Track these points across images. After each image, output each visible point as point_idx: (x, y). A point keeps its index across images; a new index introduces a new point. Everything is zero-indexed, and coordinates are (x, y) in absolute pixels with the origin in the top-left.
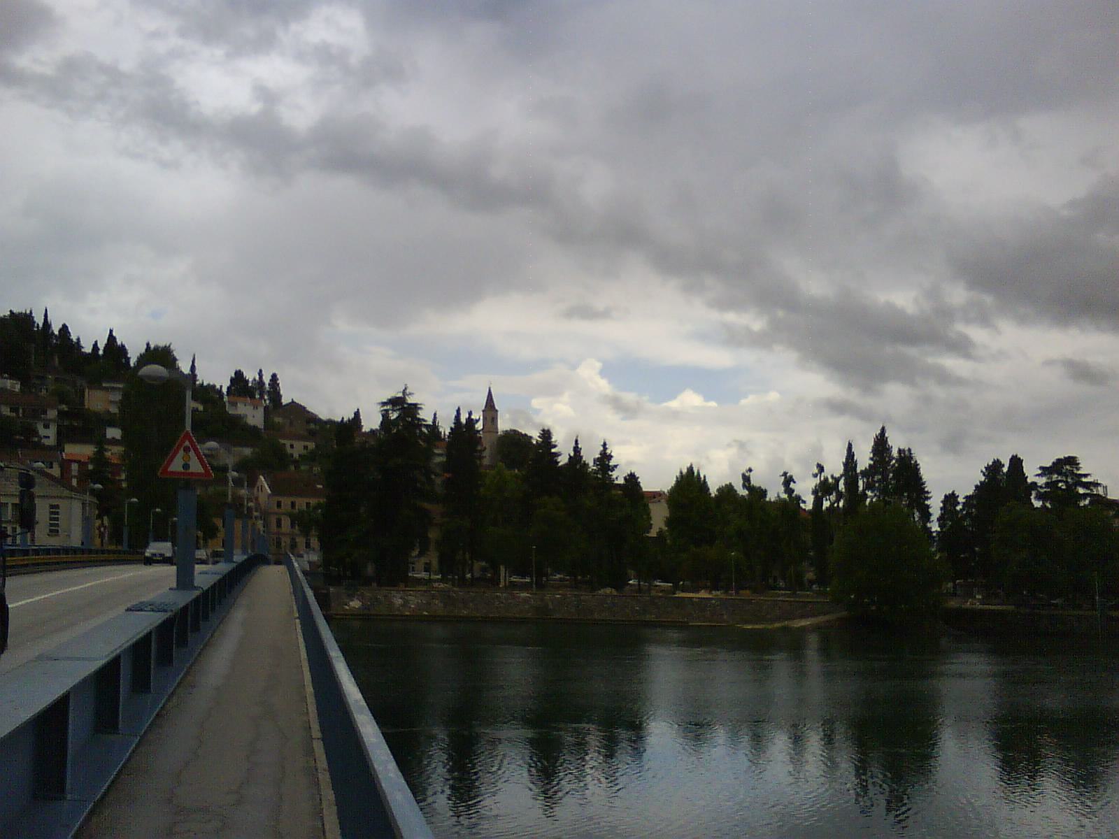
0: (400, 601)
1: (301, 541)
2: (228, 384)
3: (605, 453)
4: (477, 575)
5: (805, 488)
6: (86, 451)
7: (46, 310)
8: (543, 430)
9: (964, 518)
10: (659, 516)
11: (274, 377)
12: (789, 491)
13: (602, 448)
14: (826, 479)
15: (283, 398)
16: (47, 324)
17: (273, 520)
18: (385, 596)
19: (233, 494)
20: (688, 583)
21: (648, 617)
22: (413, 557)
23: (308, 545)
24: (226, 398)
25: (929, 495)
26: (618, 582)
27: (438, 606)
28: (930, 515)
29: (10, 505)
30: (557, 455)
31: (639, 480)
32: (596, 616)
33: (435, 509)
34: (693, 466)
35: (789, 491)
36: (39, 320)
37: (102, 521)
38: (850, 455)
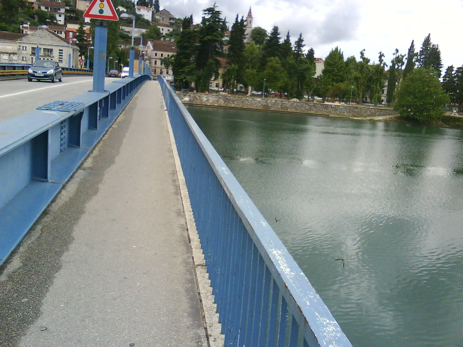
0: (206, 99)
1: (165, 71)
3: (301, 39)
4: (238, 89)
5: (388, 60)
6: (76, 27)
8: (275, 27)
9: (455, 77)
10: (319, 69)
12: (381, 61)
13: (299, 37)
14: (399, 56)
15: (160, 8)
18: (199, 97)
20: (329, 98)
21: (312, 112)
22: (212, 81)
23: (167, 73)
24: (136, 7)
25: (442, 66)
26: (299, 96)
27: (222, 102)
28: (441, 75)
30: (279, 38)
32: (289, 110)
33: (223, 60)
34: (338, 47)
35: (381, 61)
37: (82, 58)
38: (412, 46)
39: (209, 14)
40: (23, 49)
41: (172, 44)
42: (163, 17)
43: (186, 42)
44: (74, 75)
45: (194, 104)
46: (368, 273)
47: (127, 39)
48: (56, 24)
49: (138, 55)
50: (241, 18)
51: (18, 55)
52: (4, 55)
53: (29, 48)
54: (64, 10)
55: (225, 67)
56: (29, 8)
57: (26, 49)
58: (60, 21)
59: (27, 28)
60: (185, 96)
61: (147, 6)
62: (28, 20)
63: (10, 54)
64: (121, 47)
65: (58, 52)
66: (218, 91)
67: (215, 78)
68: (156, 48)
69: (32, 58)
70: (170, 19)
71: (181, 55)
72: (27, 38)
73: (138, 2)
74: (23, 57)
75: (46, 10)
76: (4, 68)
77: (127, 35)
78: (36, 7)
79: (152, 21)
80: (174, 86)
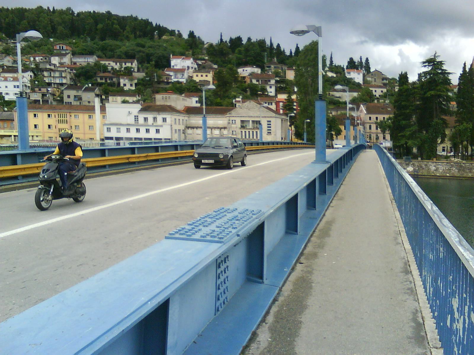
1: (381, 136)
2: (347, 64)
7: (271, 38)
11: (367, 59)
16: (271, 44)
17: (367, 126)
18: (426, 165)
19: (349, 114)
23: (384, 138)
24: (346, 71)
27: (455, 171)
33: (451, 120)
36: (268, 43)
39: (429, 66)
40: (232, 122)
41: (387, 105)
42: (375, 78)
43: (404, 101)
44: (263, 151)
45: (420, 175)
47: (338, 104)
48: (267, 95)
49: (353, 122)
50: (469, 67)
51: (228, 129)
55: (455, 127)
56: (241, 82)
57: (235, 123)
58: (271, 92)
59: (239, 101)
60: (408, 165)
61: (357, 69)
62: (240, 93)
63: (221, 128)
64: (331, 113)
65: (266, 123)
66: (447, 157)
67: (441, 141)
68: (369, 111)
70: (383, 79)
71: (400, 116)
73: (347, 66)
74: (233, 131)
75: (258, 83)
76: (13, 159)
77: (339, 101)
78: (248, 81)
79: (363, 83)
80: (394, 154)
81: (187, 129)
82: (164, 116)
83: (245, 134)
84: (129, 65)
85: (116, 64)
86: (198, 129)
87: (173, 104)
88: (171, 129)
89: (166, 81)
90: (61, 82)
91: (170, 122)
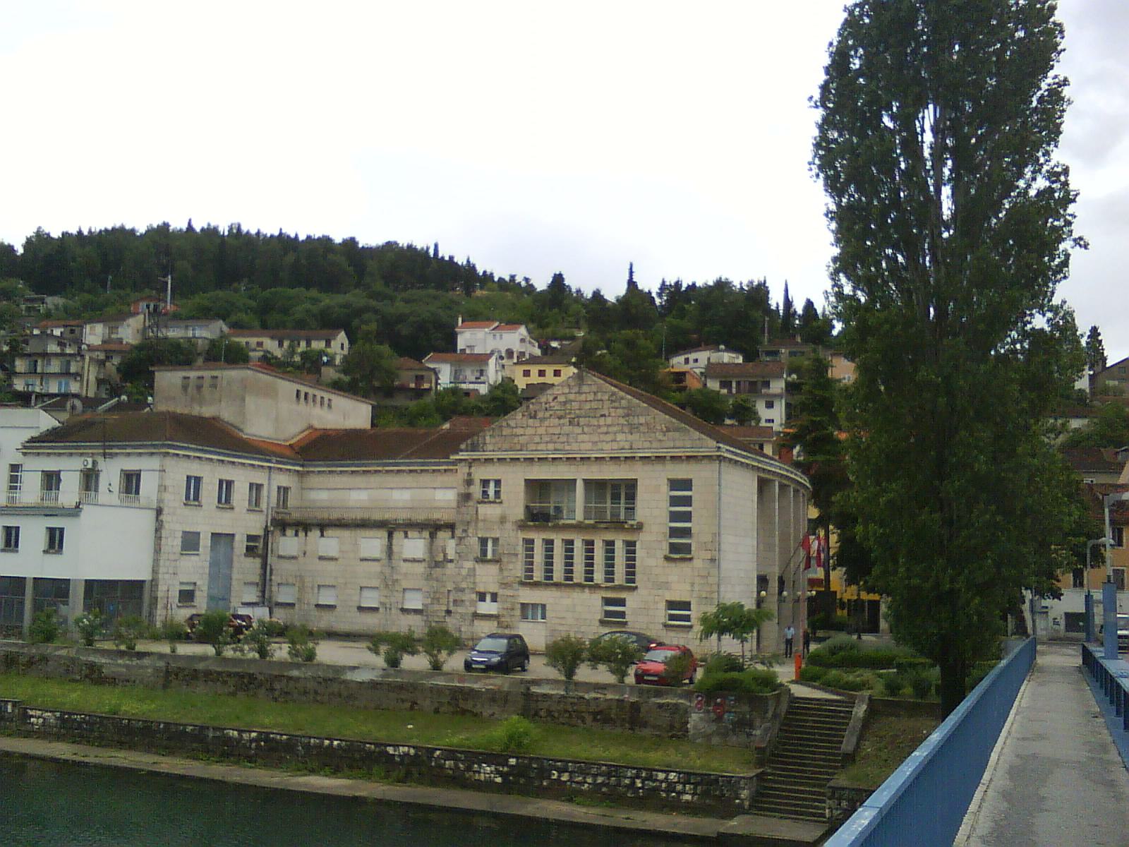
16: (788, 303)
29: (580, 486)
31: (649, 283)
36: (776, 299)
40: (485, 493)
46: (822, 533)
52: (406, 537)
53: (514, 482)
54: (783, 385)
57: (497, 493)
65: (665, 492)
69: (529, 543)
72: (506, 432)
74: (484, 542)
81: (278, 533)
82: (131, 464)
83: (590, 558)
84: (318, 345)
85: (281, 345)
86: (329, 532)
87: (226, 412)
88: (159, 529)
89: (412, 385)
90: (63, 391)
91: (154, 498)
